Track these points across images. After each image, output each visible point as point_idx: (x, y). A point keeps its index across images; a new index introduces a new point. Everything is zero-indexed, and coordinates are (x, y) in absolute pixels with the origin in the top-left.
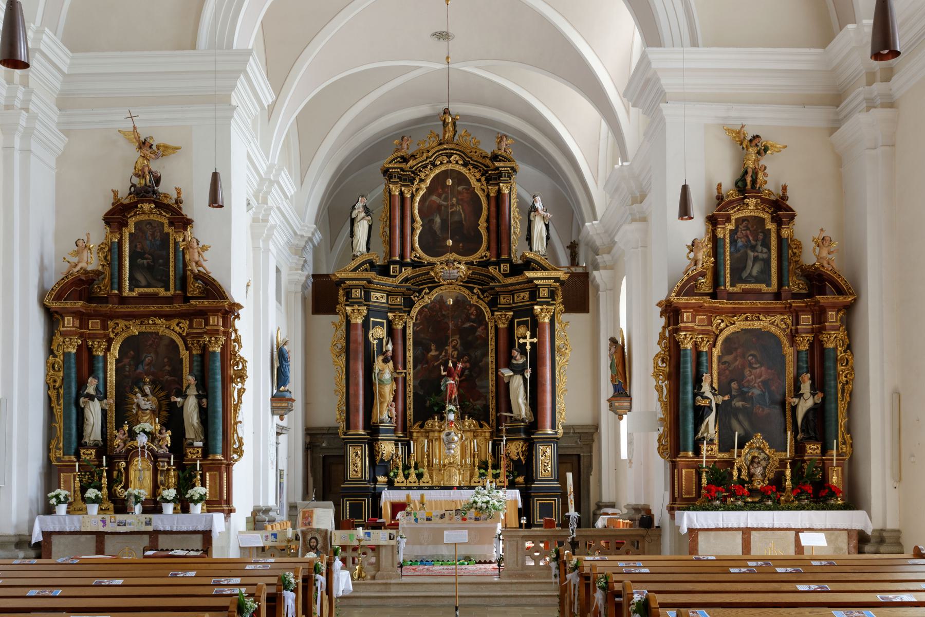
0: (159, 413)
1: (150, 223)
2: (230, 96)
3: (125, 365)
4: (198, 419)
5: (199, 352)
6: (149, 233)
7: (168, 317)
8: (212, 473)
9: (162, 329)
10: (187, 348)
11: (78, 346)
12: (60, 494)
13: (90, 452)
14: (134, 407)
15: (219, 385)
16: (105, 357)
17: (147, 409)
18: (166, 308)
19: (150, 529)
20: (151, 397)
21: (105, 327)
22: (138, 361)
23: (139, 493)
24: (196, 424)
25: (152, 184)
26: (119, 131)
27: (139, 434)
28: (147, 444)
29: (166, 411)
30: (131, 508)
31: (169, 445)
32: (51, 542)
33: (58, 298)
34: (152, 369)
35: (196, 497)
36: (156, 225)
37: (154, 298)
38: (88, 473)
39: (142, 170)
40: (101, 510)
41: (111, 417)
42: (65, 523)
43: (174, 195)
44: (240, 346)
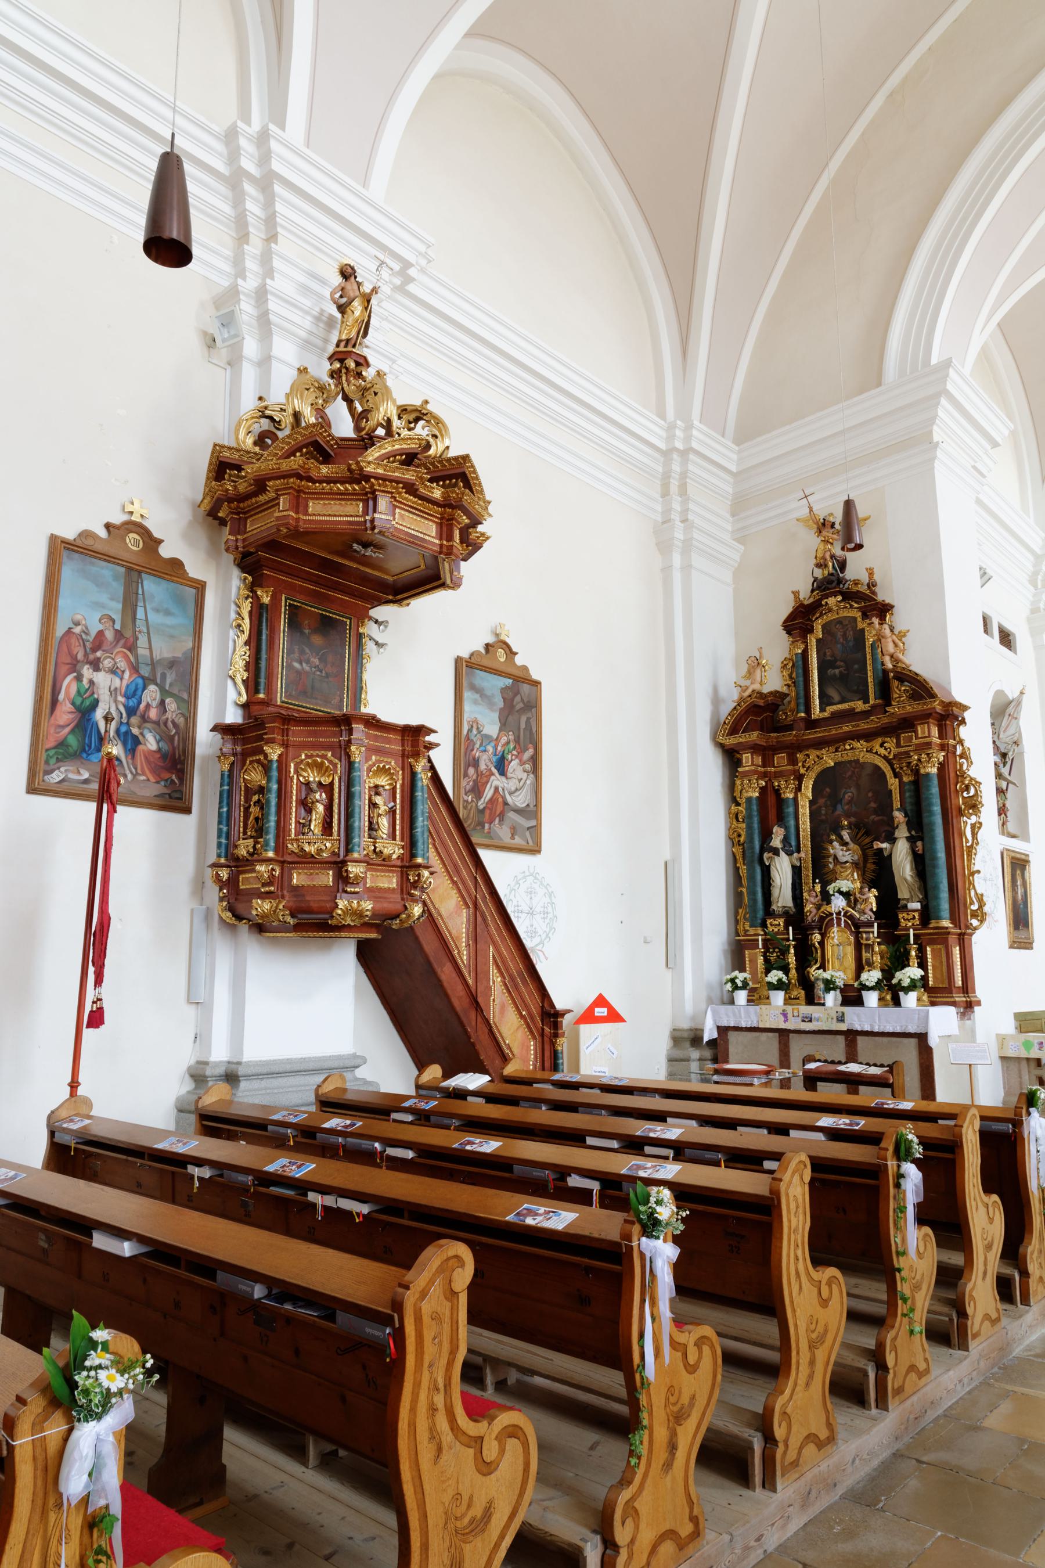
0: (865, 867)
1: (839, 621)
2: (931, 432)
3: (820, 807)
4: (912, 869)
5: (911, 778)
6: (839, 634)
7: (868, 736)
8: (935, 946)
9: (862, 754)
10: (896, 775)
11: (760, 788)
12: (736, 978)
13: (777, 923)
14: (831, 860)
15: (938, 820)
16: (795, 799)
17: (847, 862)
18: (863, 726)
19: (843, 1027)
20: (852, 845)
21: (793, 761)
22: (835, 800)
23: (832, 976)
24: (909, 878)
25: (836, 571)
26: (797, 520)
27: (834, 895)
28: (843, 909)
29: (874, 863)
30: (819, 998)
31: (875, 910)
32: (728, 1040)
33: (733, 731)
34: (854, 809)
35: (906, 983)
36: (847, 622)
37: (850, 715)
38: (777, 950)
39: (824, 558)
40: (788, 1001)
41: (807, 875)
42: (741, 1017)
43: (865, 579)
44: (970, 763)
